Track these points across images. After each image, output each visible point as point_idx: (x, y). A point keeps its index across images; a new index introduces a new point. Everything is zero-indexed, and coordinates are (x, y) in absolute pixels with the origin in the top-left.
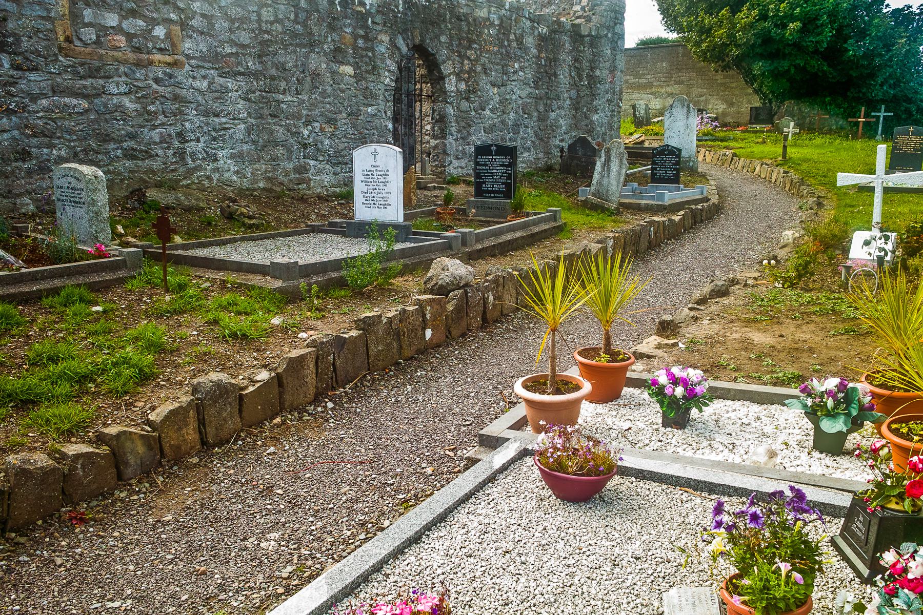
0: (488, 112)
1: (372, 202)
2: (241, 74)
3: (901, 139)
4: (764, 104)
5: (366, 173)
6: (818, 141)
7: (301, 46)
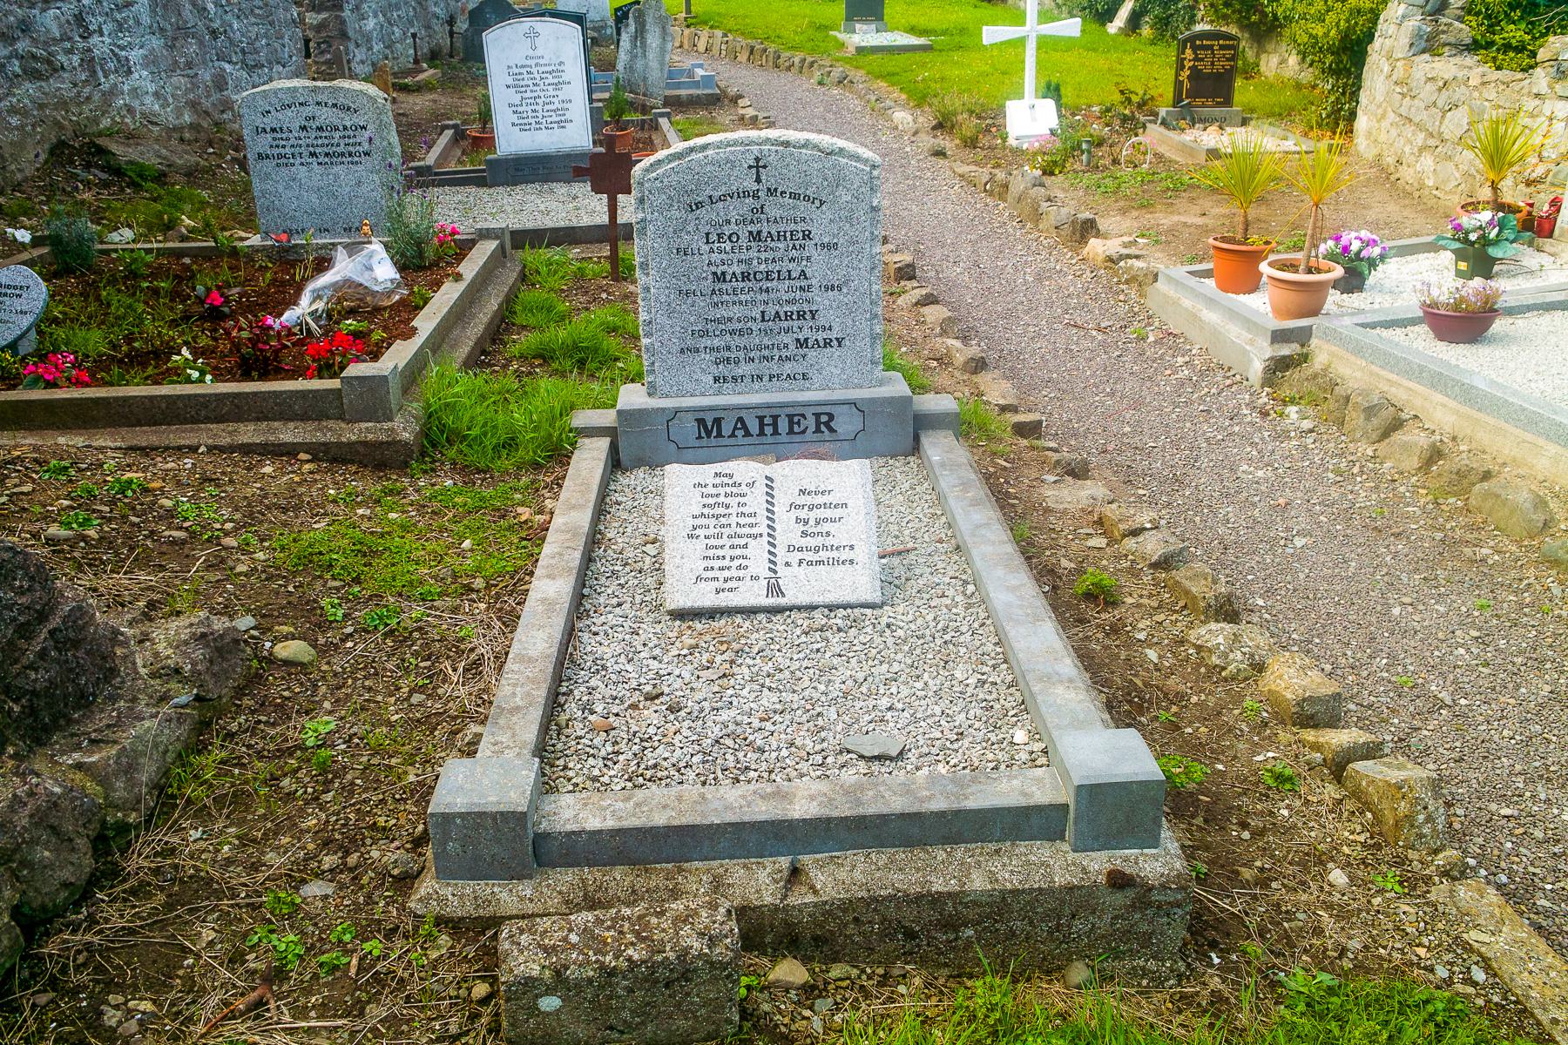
1: (533, 121)
5: (517, 71)
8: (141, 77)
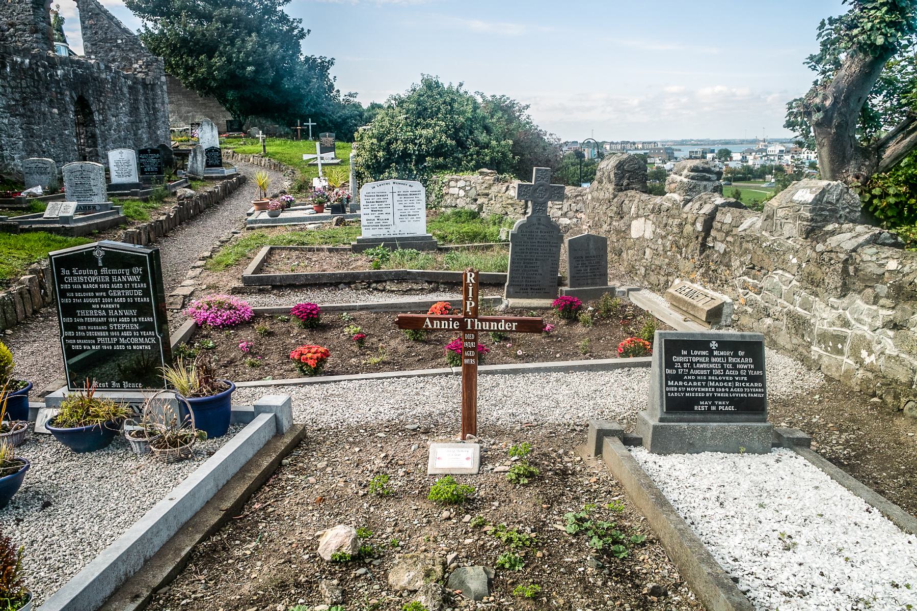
0: (112, 132)
2: (18, 115)
3: (323, 139)
4: (235, 118)
6: (278, 142)
7: (37, 99)
8: (18, 161)
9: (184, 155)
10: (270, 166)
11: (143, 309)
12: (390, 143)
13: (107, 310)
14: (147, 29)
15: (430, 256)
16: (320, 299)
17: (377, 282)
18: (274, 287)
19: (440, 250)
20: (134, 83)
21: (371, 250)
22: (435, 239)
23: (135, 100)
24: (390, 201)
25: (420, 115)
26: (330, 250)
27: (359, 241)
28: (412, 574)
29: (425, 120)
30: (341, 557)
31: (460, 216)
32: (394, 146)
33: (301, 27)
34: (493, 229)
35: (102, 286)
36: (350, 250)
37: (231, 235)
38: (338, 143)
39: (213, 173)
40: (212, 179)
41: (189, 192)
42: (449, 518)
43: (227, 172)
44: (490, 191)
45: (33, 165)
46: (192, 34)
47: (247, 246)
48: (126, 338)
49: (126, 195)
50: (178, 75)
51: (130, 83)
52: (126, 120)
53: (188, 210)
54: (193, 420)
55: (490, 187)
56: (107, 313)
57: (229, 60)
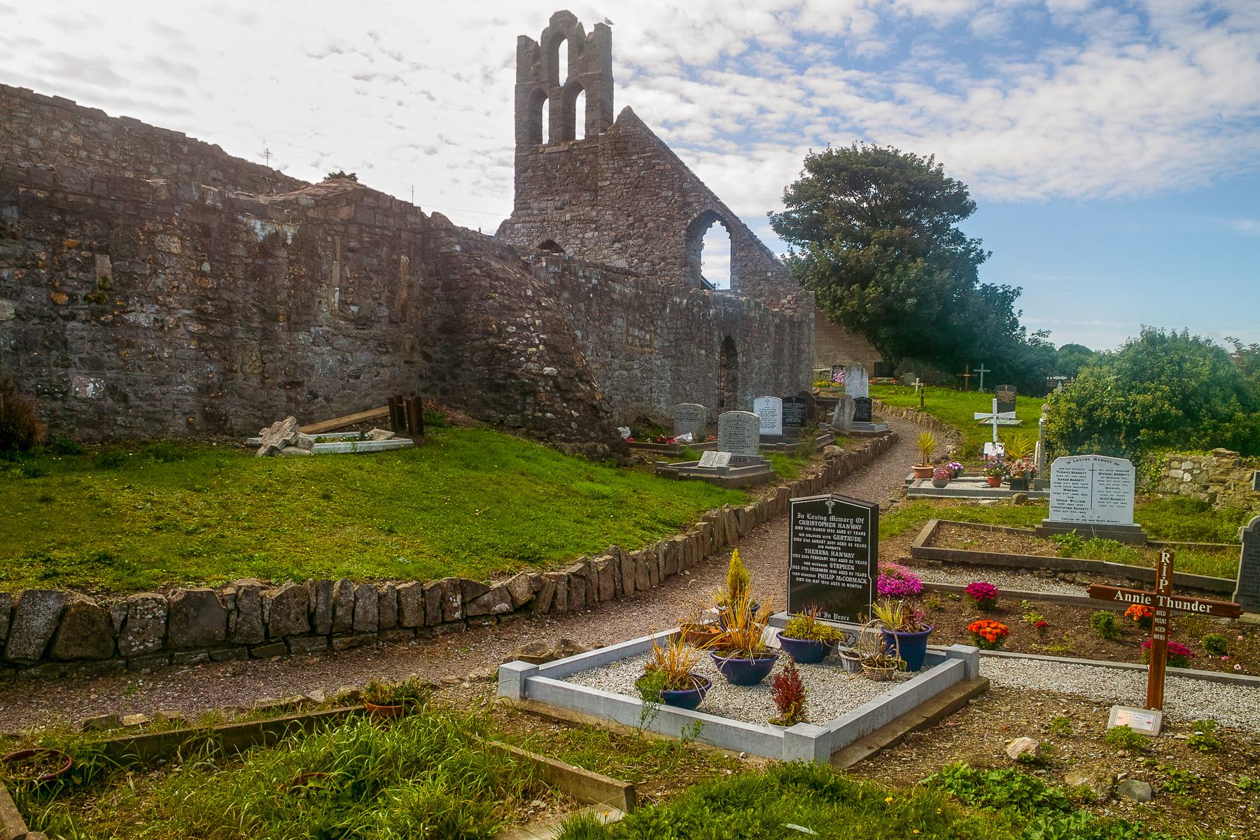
6: (939, 393)
8: (663, 405)
9: (828, 404)
10: (928, 423)
11: (861, 554)
12: (1093, 409)
13: (830, 551)
14: (792, 253)
15: (1136, 551)
16: (1000, 582)
17: (1065, 572)
18: (945, 563)
19: (1151, 545)
20: (781, 321)
21: (1059, 536)
22: (1144, 531)
23: (780, 340)
24: (1088, 480)
25: (1135, 376)
26: (1009, 532)
27: (1045, 524)
28: (1086, 779)
29: (1142, 382)
30: (1026, 758)
31: (1183, 507)
32: (1098, 413)
33: (980, 247)
34: (1227, 526)
35: (829, 531)
36: (1033, 534)
37: (889, 504)
38: (1020, 398)
39: (860, 429)
40: (859, 435)
41: (838, 449)
42: (1123, 757)
43: (878, 428)
44: (1228, 478)
45: (684, 411)
46: (845, 260)
47: (911, 517)
48: (842, 576)
49: (771, 448)
50: (823, 307)
51: (777, 321)
52: (768, 362)
53: (836, 471)
54: (897, 650)
55: (1227, 472)
56: (830, 553)
57: (887, 291)
